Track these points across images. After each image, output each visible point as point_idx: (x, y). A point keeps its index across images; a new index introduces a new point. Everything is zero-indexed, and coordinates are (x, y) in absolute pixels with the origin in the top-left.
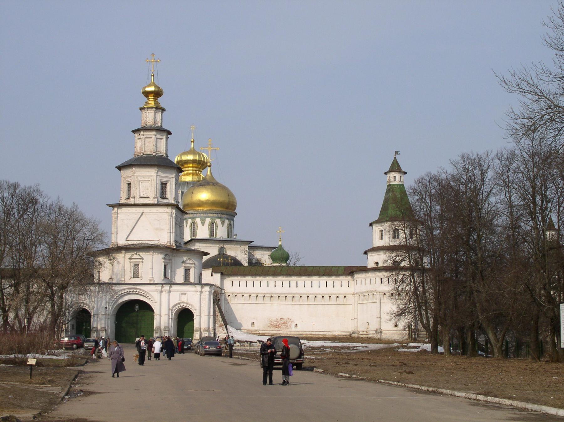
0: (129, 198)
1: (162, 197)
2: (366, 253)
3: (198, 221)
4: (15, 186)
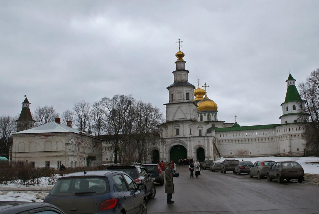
0: (172, 101)
1: (187, 100)
3: (203, 114)
4: (122, 97)
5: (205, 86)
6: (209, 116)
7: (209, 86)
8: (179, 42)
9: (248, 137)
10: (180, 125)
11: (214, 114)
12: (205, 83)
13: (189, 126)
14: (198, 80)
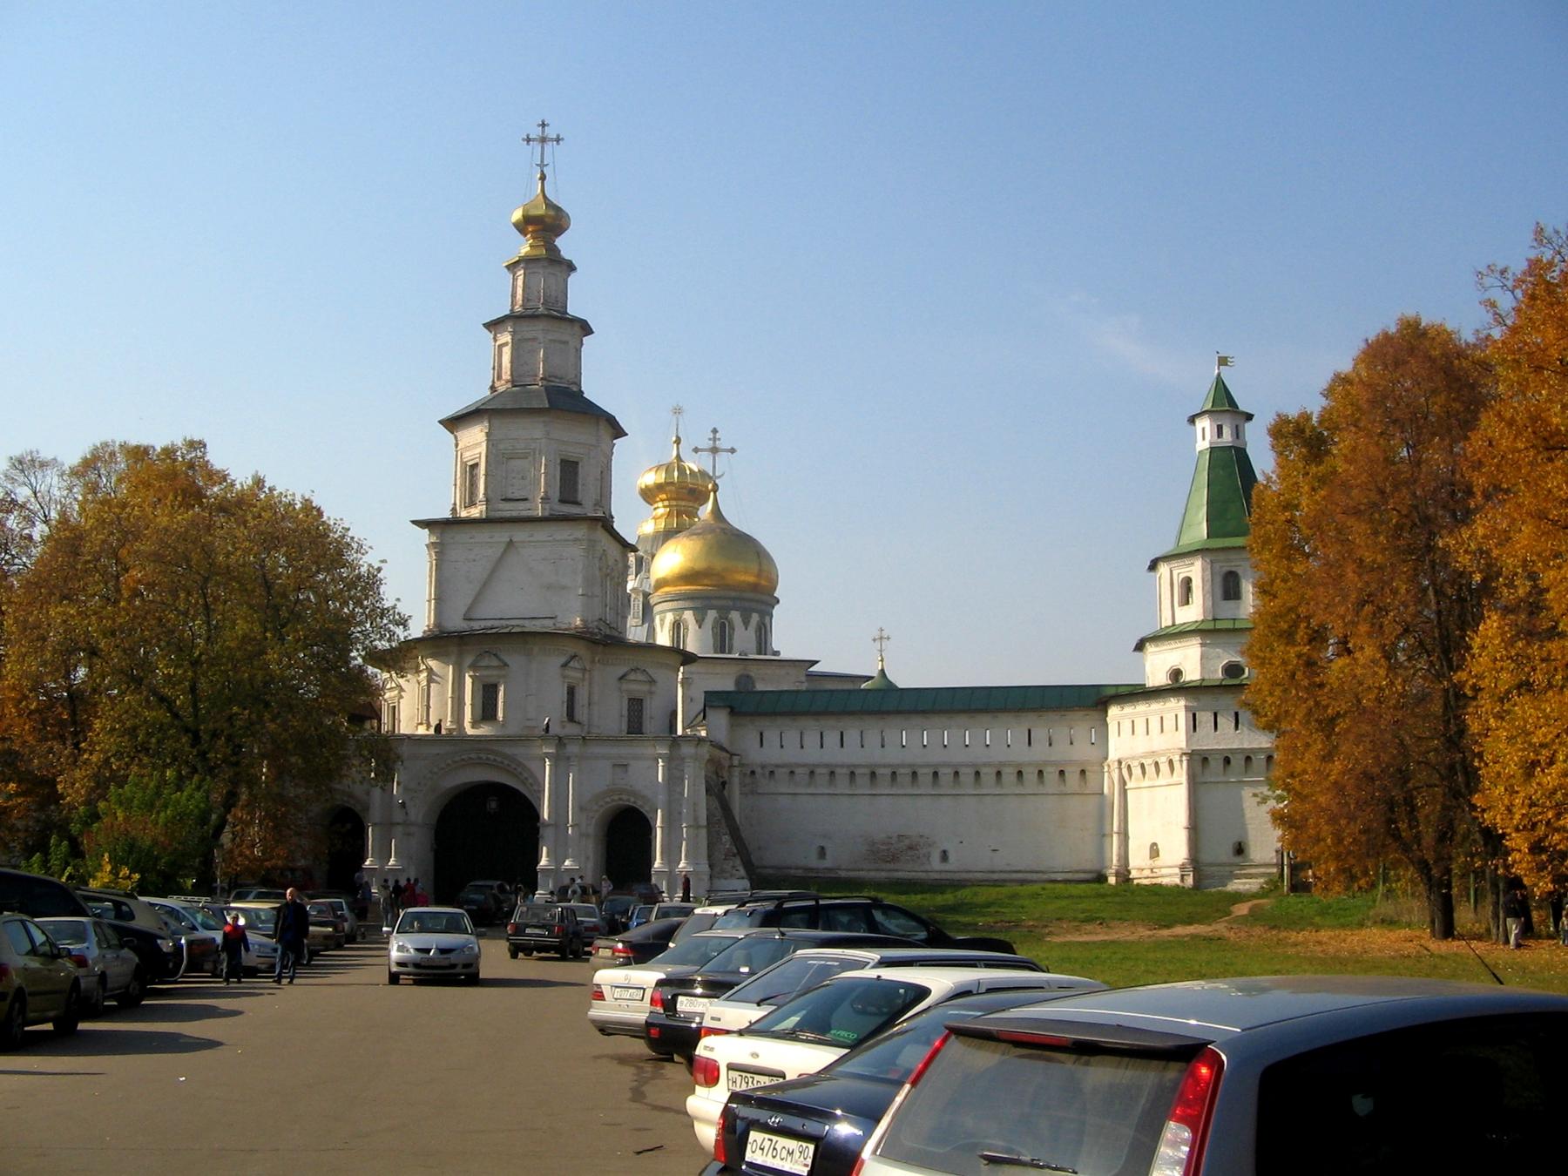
1: (562, 501)
2: (1140, 647)
5: (714, 450)
6: (723, 625)
7: (733, 451)
8: (543, 140)
9: (936, 756)
10: (507, 659)
11: (755, 618)
12: (715, 431)
13: (565, 665)
14: (678, 411)
